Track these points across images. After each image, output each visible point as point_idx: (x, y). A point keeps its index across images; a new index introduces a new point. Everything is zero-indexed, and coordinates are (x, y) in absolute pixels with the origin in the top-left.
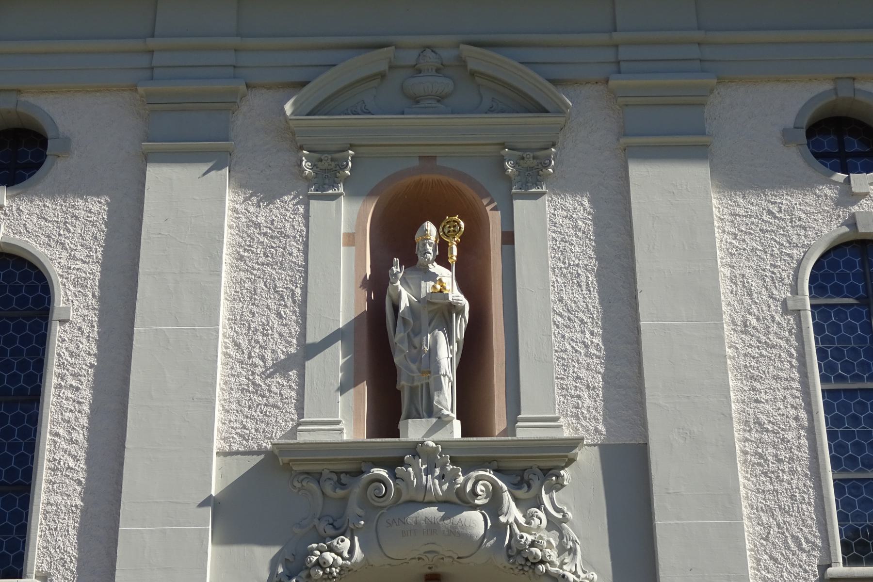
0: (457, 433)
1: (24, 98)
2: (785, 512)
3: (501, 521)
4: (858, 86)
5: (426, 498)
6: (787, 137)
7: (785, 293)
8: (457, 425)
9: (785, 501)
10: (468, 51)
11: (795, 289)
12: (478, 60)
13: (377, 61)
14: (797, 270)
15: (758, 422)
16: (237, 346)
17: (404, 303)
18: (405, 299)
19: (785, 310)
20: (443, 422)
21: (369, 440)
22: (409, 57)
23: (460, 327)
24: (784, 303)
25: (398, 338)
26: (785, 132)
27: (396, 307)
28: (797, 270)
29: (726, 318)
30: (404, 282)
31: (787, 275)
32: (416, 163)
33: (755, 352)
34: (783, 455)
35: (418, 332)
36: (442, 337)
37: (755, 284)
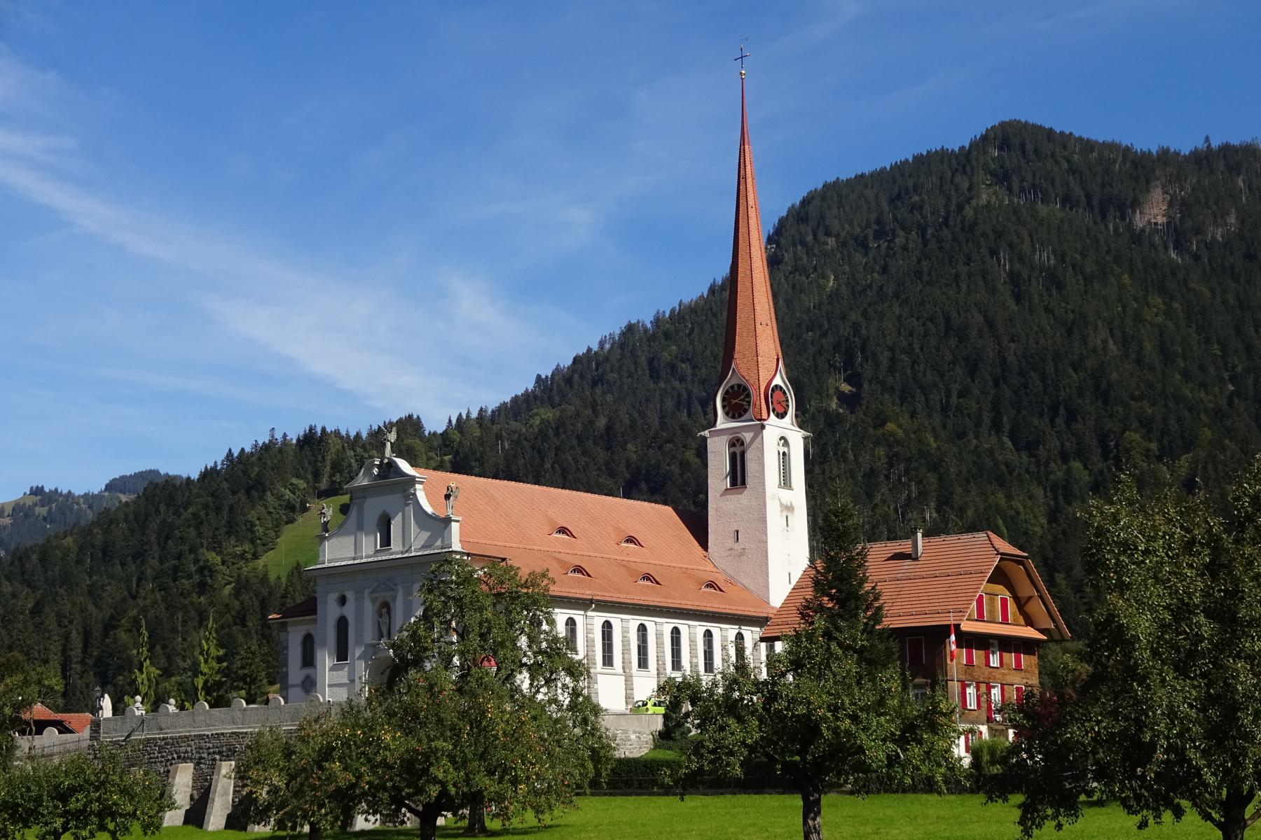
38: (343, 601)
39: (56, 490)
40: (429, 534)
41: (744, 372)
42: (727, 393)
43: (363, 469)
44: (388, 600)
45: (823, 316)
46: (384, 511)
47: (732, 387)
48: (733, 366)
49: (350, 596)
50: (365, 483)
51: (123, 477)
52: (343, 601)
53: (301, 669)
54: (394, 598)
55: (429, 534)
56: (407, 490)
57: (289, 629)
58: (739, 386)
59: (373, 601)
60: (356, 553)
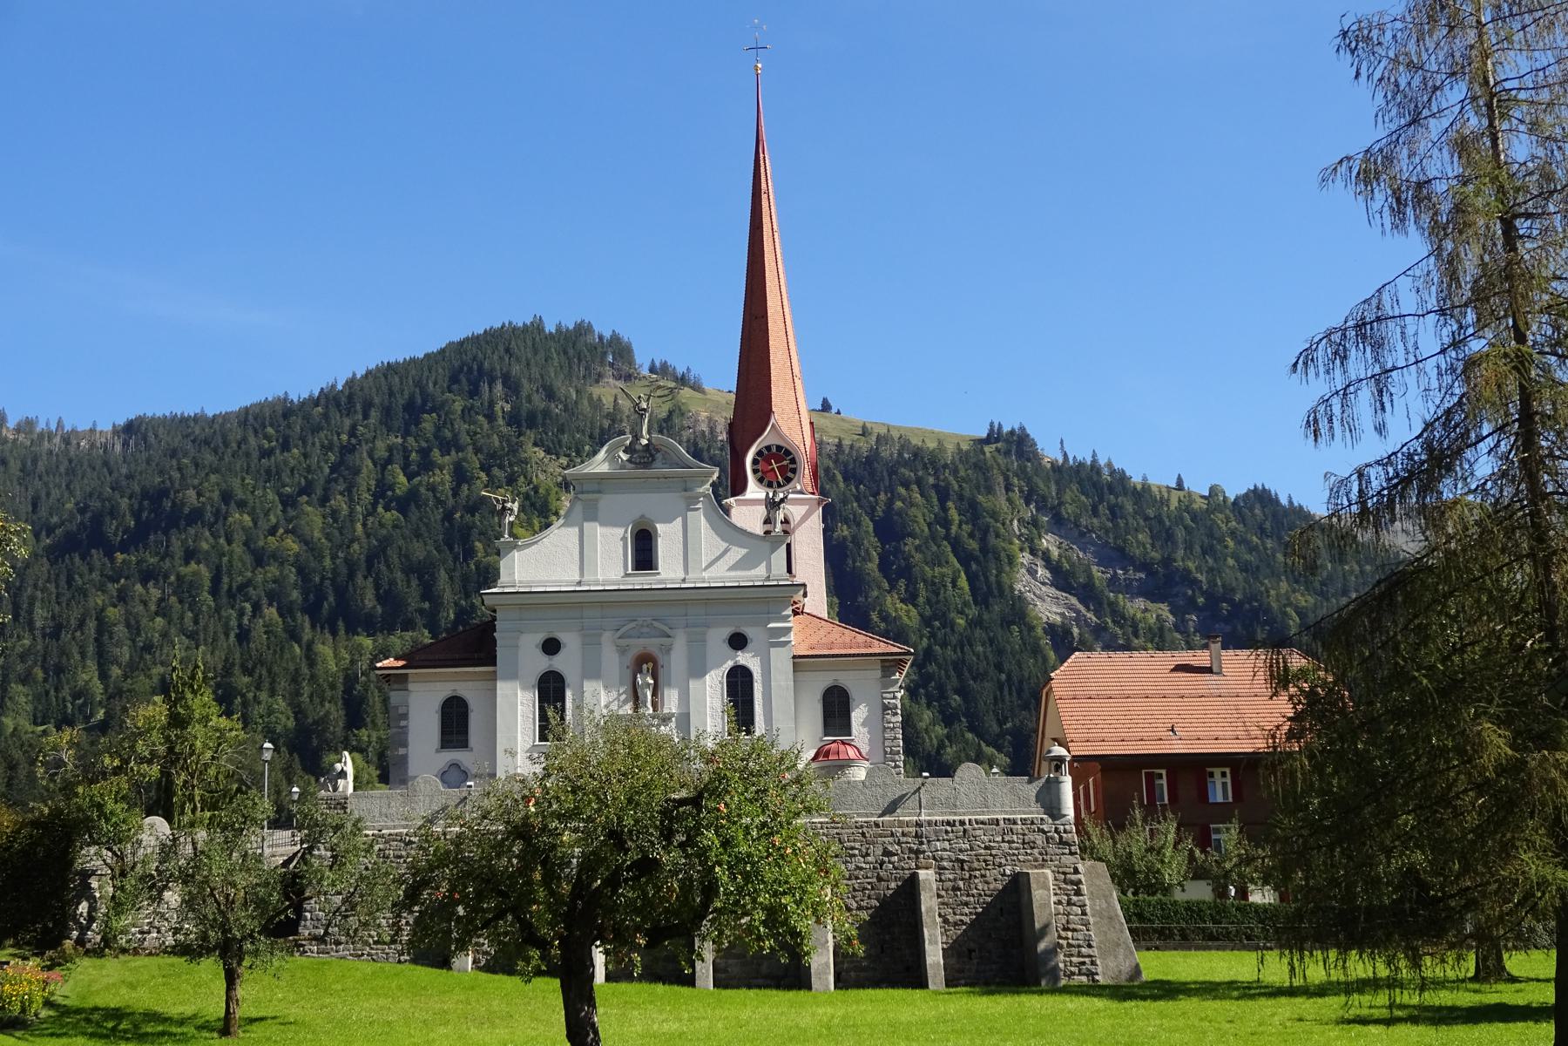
38: (551, 647)
39: (583, 321)
40: (744, 551)
41: (785, 430)
42: (759, 453)
43: (605, 448)
44: (655, 651)
45: (60, 475)
46: (643, 516)
47: (768, 448)
48: (772, 421)
49: (570, 640)
50: (604, 468)
51: (390, 369)
52: (551, 647)
53: (437, 751)
54: (668, 650)
55: (744, 551)
56: (691, 489)
57: (411, 686)
58: (779, 448)
59: (622, 651)
60: (582, 574)
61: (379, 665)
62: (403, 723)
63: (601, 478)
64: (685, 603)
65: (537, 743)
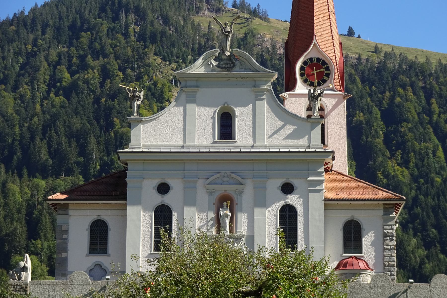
0: (229, 234)
1: (166, 180)
2: (272, 244)
3: (375, 237)
4: (290, 180)
5: (344, 173)
6: (278, 188)
7: (275, 213)
8: (229, 232)
9: (272, 243)
10: (232, 174)
11: (277, 212)
12: (233, 175)
13: (218, 175)
14: (277, 210)
15: (270, 232)
16: (198, 220)
17: (222, 214)
18: (222, 213)
19: (275, 216)
20: (227, 232)
21: (219, 140)
22: (223, 174)
23: (229, 218)
24: (275, 215)
25: (221, 219)
26: (278, 187)
27: (221, 214)
28: (277, 210)
29: (266, 217)
30: (222, 211)
31: (276, 210)
32: (223, 191)
33: (270, 222)
34: (273, 237)
35: (223, 218)
36: (227, 220)
37: (271, 212)
41: (323, 48)
42: (305, 63)
43: (202, 57)
47: (311, 59)
48: (314, 41)
54: (241, 193)
57: (71, 212)
59: (210, 193)
60: (254, 141)
61: (50, 197)
62: (65, 236)
63: (199, 77)
64: (267, 161)
65: (153, 252)
